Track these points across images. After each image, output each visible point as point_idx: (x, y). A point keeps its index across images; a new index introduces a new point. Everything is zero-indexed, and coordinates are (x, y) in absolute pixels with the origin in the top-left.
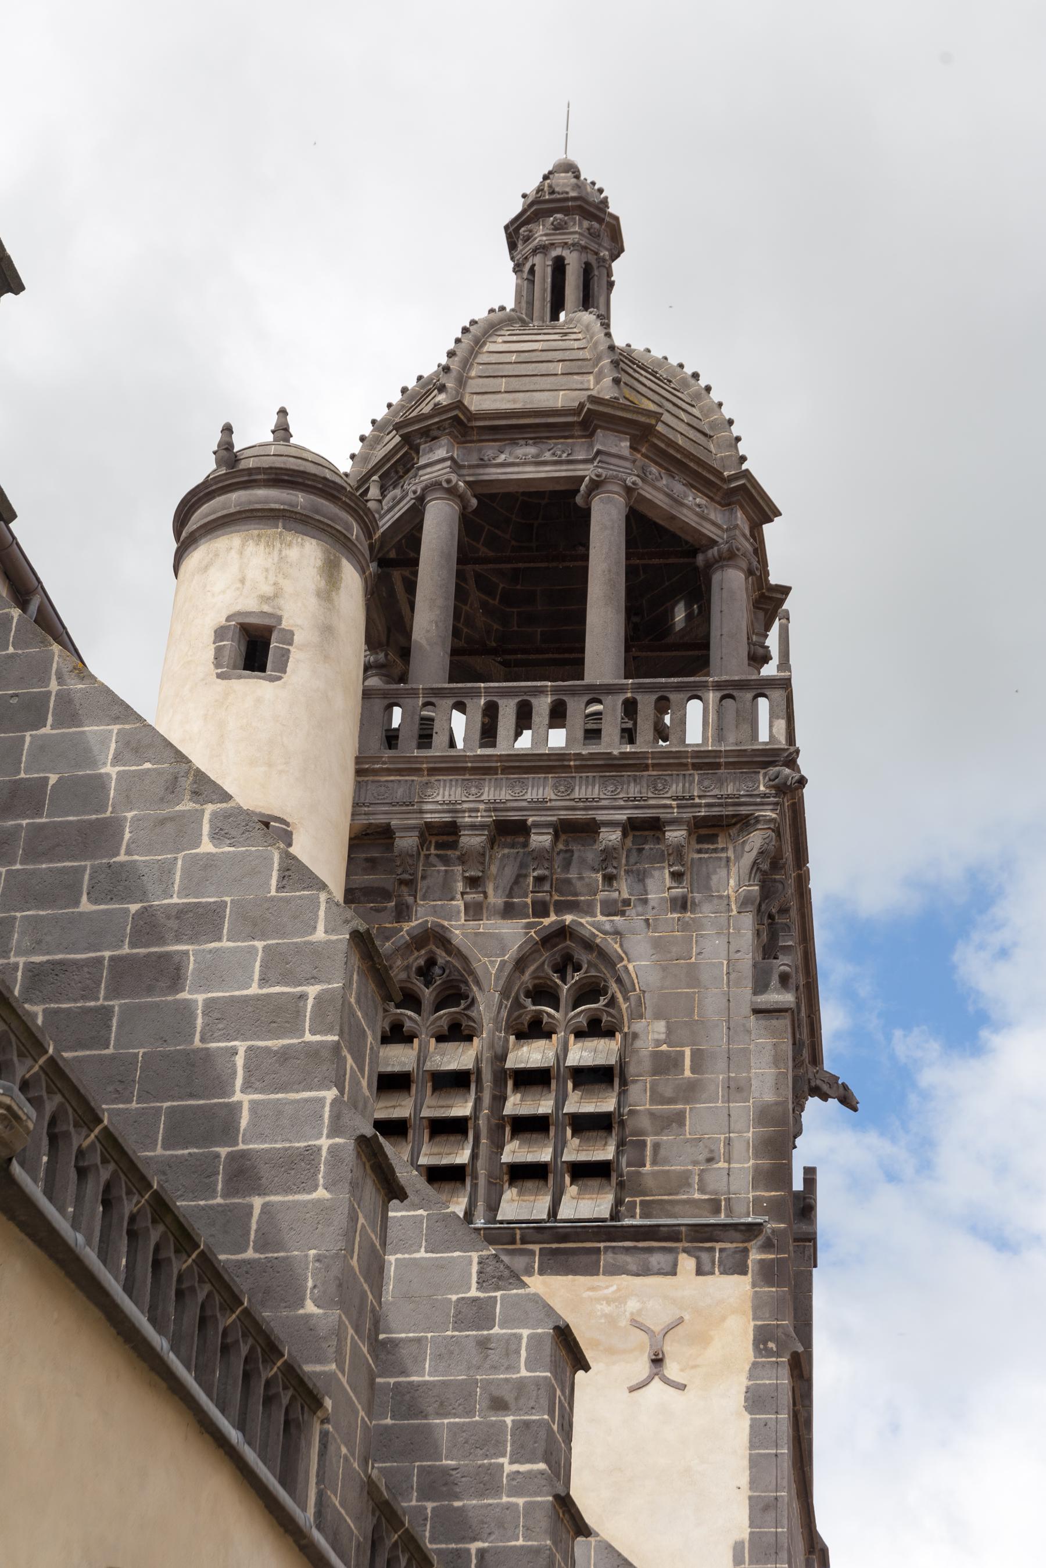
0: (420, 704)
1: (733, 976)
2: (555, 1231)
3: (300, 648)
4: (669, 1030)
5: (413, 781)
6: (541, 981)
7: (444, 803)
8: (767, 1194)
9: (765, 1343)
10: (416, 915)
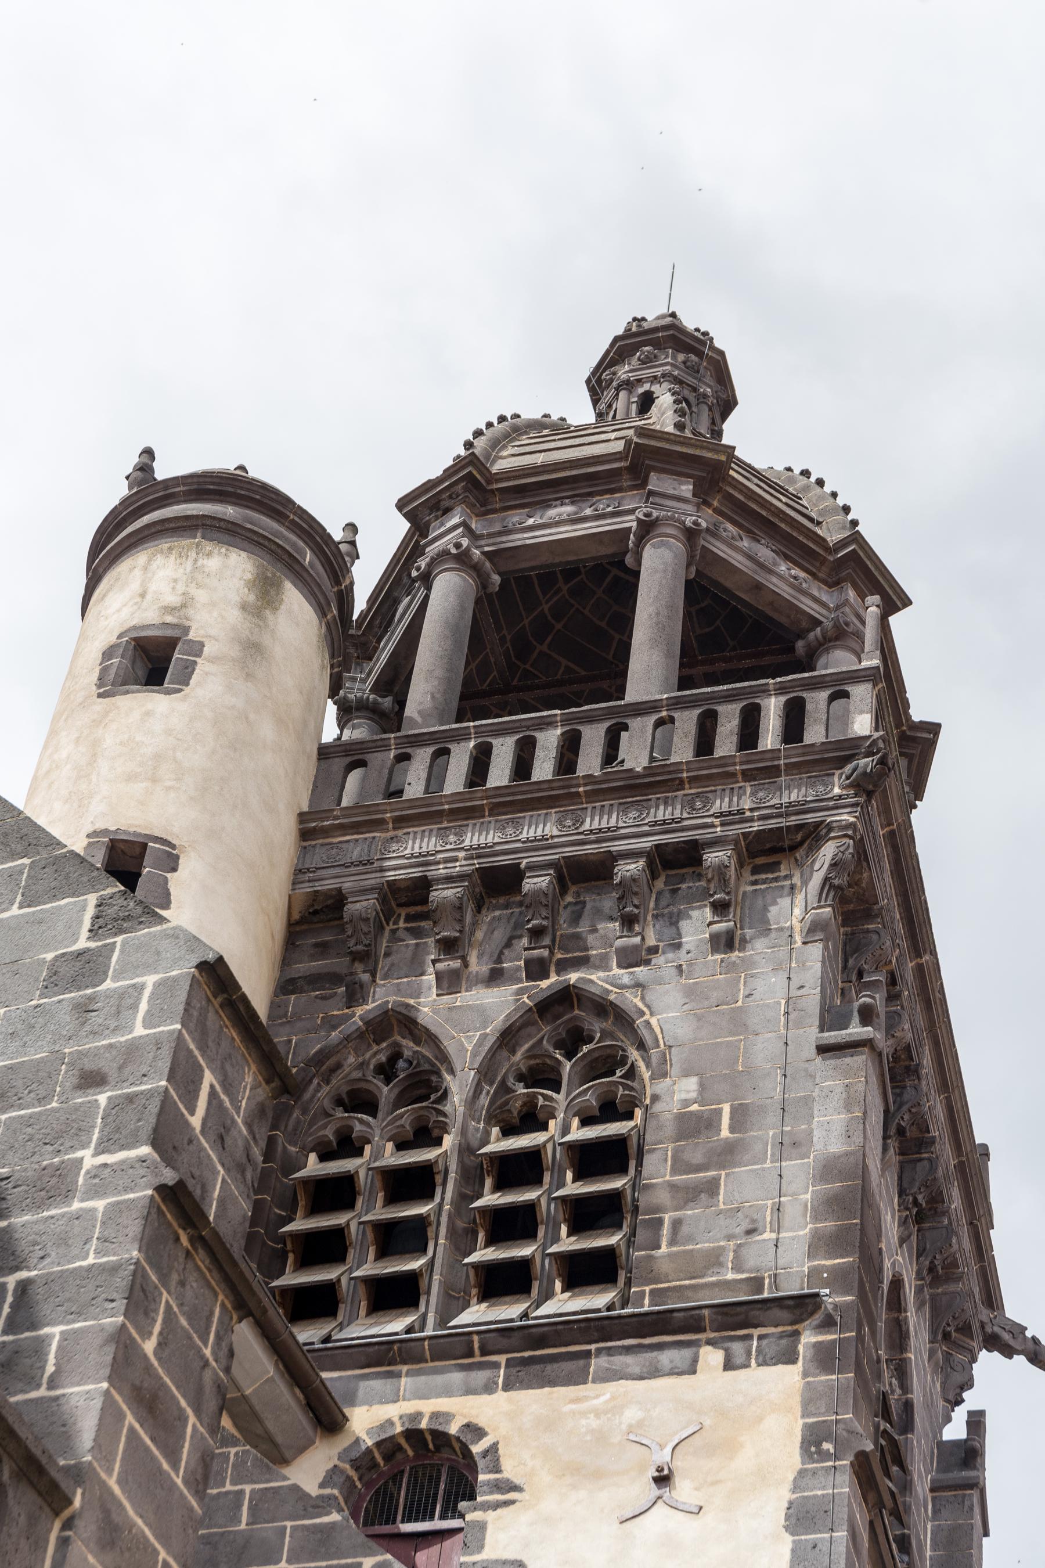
0: (392, 756)
1: (792, 1017)
2: (526, 1331)
3: (213, 660)
4: (702, 1087)
5: (374, 838)
6: (538, 1061)
7: (412, 856)
8: (828, 1263)
9: (818, 1444)
10: (374, 997)
